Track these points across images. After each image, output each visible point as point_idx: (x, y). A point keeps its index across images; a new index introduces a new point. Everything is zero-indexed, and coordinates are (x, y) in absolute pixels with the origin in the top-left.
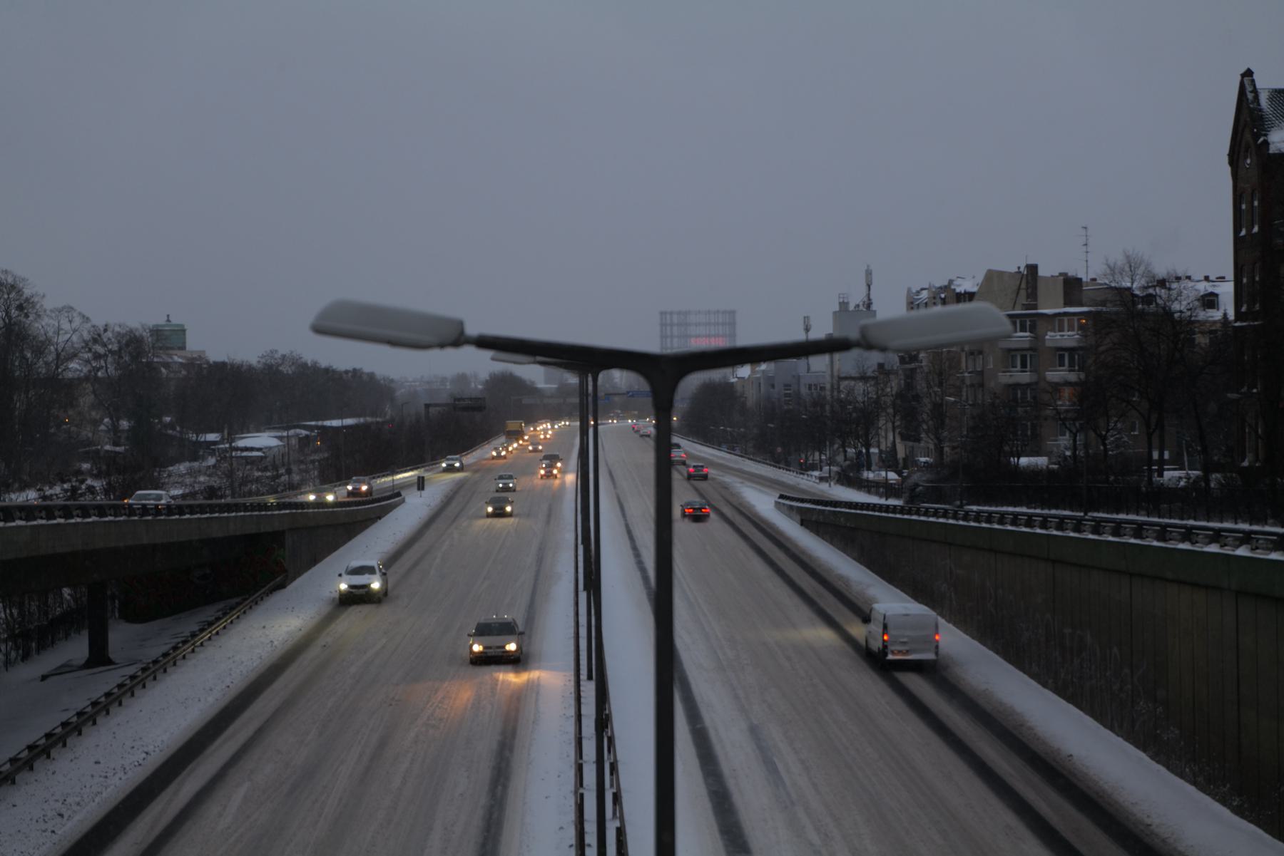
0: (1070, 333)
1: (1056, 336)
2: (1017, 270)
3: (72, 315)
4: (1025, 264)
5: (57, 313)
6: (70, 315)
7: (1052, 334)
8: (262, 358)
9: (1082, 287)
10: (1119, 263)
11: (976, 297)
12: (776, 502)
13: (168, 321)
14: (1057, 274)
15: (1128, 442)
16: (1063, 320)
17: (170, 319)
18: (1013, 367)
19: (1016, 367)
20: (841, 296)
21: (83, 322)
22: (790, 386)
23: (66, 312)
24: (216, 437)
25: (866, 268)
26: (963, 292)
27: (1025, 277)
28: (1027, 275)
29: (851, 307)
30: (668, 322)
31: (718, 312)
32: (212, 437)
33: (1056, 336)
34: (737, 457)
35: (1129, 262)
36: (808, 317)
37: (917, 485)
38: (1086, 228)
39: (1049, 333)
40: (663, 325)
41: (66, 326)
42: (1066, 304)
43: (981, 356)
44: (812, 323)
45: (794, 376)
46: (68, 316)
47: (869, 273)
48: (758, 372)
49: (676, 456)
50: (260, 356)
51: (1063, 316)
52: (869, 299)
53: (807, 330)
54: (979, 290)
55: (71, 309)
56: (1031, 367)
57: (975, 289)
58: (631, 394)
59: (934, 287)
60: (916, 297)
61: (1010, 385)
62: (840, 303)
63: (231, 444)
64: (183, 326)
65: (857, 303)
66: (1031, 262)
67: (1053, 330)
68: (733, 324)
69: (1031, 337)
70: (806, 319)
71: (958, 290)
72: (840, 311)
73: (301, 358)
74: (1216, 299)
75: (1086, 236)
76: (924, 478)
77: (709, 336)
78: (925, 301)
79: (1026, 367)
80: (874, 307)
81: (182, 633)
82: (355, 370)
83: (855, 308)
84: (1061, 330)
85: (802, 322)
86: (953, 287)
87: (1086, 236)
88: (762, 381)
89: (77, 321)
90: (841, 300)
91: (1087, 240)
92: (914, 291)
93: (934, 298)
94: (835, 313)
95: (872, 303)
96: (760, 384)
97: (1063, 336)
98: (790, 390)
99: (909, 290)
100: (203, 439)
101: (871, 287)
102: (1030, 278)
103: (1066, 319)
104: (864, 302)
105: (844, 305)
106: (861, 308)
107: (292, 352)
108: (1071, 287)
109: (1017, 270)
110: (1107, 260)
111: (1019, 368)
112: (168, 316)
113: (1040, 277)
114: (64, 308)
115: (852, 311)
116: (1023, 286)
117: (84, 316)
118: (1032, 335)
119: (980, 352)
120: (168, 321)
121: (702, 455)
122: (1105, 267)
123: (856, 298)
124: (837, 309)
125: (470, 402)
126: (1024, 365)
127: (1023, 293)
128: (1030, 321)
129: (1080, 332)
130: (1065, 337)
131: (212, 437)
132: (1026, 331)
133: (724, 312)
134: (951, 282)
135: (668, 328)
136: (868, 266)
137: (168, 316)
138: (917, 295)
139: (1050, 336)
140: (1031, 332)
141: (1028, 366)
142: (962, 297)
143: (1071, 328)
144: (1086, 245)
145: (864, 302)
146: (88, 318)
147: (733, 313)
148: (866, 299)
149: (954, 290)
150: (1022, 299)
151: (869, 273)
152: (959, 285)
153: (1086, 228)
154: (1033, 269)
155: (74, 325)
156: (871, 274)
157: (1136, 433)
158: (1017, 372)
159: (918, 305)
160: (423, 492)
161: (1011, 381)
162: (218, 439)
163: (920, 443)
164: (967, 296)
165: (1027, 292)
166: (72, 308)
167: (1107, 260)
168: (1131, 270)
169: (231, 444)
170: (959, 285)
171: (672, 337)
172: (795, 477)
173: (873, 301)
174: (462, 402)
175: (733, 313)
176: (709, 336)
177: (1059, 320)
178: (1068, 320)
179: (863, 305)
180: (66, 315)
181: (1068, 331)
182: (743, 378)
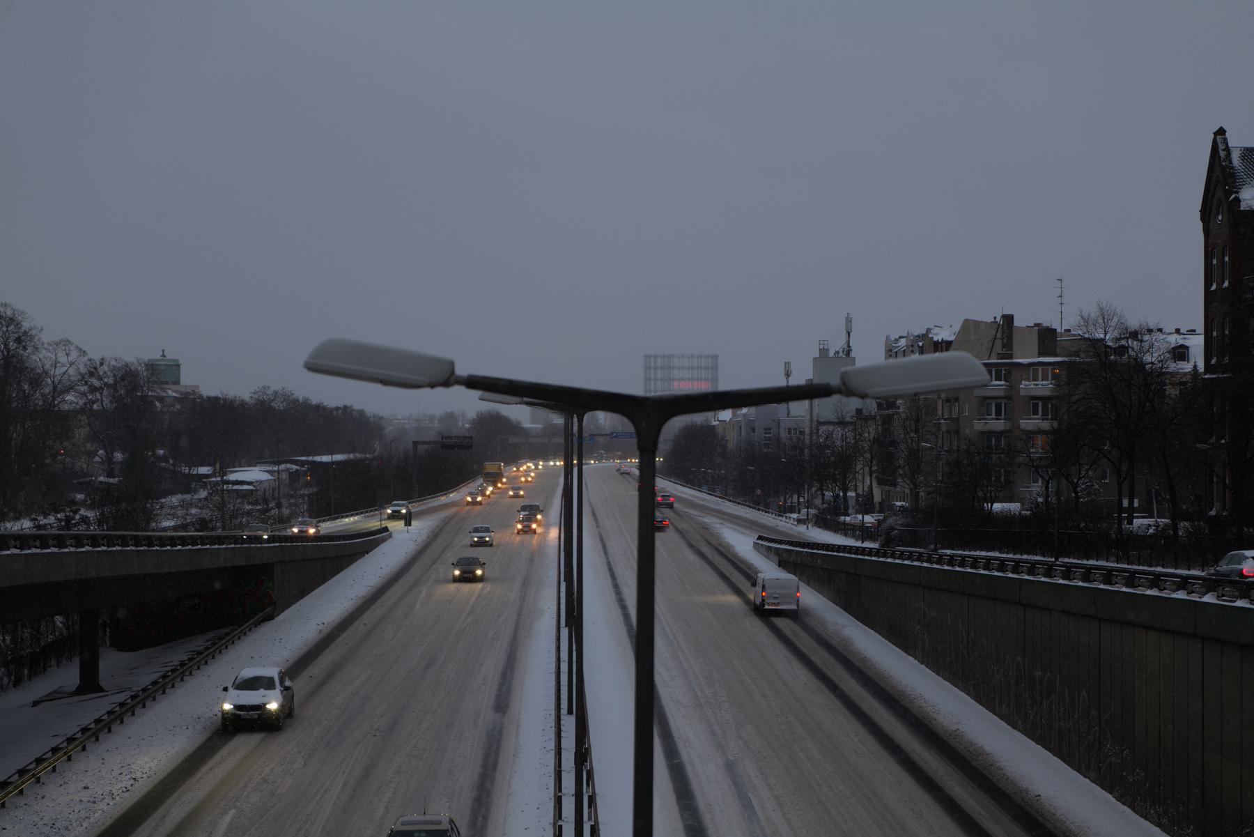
2: (993, 320)
5: (55, 346)
7: (1027, 383)
11: (953, 346)
13: (163, 355)
20: (822, 342)
23: (63, 345)
29: (831, 354)
32: (204, 470)
33: (1031, 385)
37: (892, 529)
40: (647, 368)
41: (63, 359)
42: (1040, 355)
44: (792, 367)
45: (774, 420)
47: (849, 321)
52: (849, 346)
53: (788, 375)
55: (67, 342)
56: (1005, 416)
57: (952, 338)
58: (615, 434)
62: (820, 349)
63: (222, 478)
67: (1028, 380)
68: (715, 368)
70: (787, 364)
73: (293, 394)
77: (692, 379)
78: (903, 349)
80: (853, 354)
81: (172, 662)
82: (345, 407)
83: (835, 354)
86: (930, 336)
89: (74, 355)
90: (822, 346)
92: (893, 339)
93: (912, 346)
95: (851, 350)
96: (741, 427)
97: (1038, 385)
98: (770, 433)
99: (888, 337)
100: (195, 472)
101: (851, 334)
103: (1040, 368)
105: (824, 351)
106: (841, 354)
107: (284, 389)
108: (1047, 337)
109: (993, 320)
111: (993, 416)
112: (163, 351)
114: (61, 341)
116: (999, 335)
117: (80, 350)
120: (163, 355)
123: (837, 344)
124: (818, 356)
126: (998, 412)
127: (999, 343)
130: (1040, 386)
131: (204, 470)
132: (1001, 380)
133: (708, 357)
134: (929, 330)
135: (652, 371)
137: (163, 351)
139: (1025, 385)
140: (1006, 380)
146: (84, 352)
147: (715, 357)
148: (845, 346)
149: (932, 338)
151: (849, 321)
152: (937, 334)
154: (1008, 319)
155: (71, 358)
156: (850, 321)
158: (992, 419)
159: (896, 352)
160: (409, 527)
161: (986, 428)
166: (69, 342)
170: (937, 334)
175: (715, 357)
176: (692, 379)
180: (63, 348)
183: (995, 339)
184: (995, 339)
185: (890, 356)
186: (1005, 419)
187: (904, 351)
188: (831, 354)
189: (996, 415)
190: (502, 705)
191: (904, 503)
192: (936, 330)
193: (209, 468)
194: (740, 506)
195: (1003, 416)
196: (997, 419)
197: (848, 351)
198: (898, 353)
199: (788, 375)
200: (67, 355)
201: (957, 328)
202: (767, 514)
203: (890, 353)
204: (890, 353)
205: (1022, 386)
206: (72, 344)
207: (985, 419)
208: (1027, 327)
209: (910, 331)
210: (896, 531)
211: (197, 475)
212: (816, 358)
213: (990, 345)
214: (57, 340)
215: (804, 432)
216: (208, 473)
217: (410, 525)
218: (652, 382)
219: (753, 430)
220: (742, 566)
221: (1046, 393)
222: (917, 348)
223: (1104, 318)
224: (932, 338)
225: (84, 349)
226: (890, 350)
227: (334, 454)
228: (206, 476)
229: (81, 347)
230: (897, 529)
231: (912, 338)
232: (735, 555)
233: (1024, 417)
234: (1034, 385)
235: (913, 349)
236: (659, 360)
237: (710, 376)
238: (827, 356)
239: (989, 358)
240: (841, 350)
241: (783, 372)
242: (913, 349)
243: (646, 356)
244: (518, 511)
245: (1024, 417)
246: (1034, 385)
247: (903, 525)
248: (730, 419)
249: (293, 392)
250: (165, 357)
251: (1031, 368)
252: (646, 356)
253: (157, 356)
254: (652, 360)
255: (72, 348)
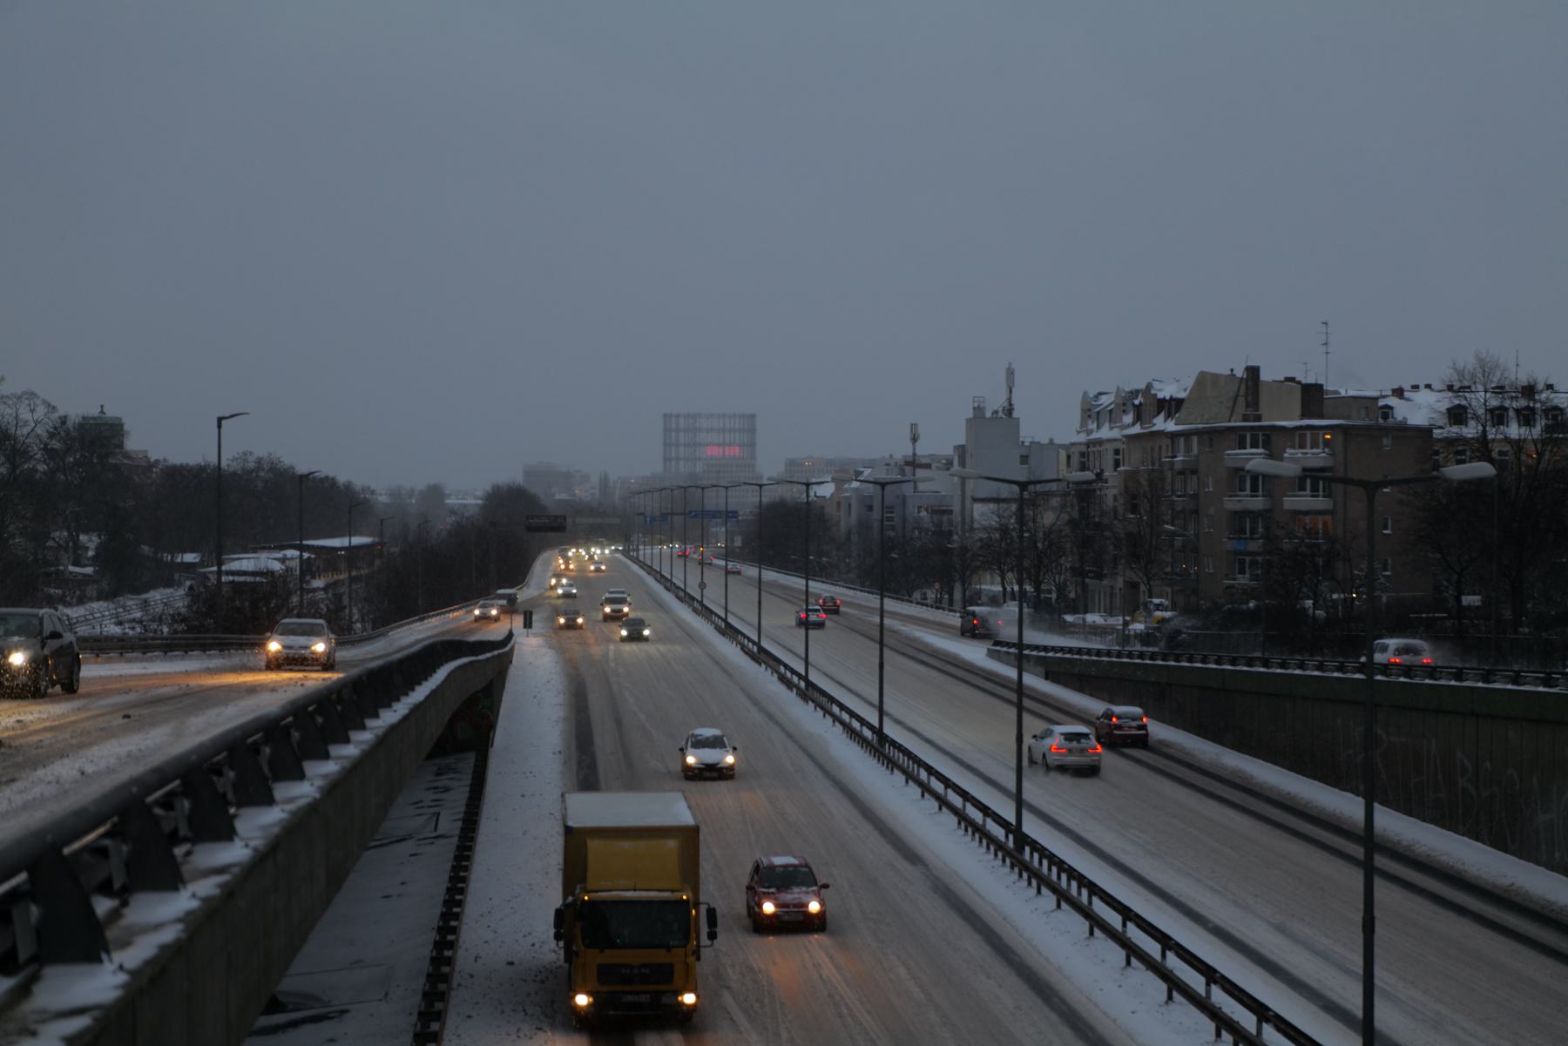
0: (1314, 451)
1: (1297, 454)
2: (1229, 373)
3: (34, 403)
4: (1244, 366)
5: (15, 400)
6: (32, 403)
7: (1293, 451)
8: (232, 460)
9: (1323, 395)
10: (1470, 367)
11: (1185, 406)
12: (989, 650)
13: (102, 412)
14: (1282, 379)
15: (1384, 584)
16: (1305, 434)
17: (105, 410)
18: (1241, 490)
19: (1245, 490)
20: (976, 399)
21: (48, 412)
22: (892, 507)
23: (26, 399)
24: (195, 558)
25: (1007, 366)
26: (1168, 398)
27: (1244, 381)
28: (1247, 379)
29: (988, 415)
30: (674, 426)
31: (734, 415)
32: (190, 558)
33: (1297, 454)
34: (866, 594)
35: (1483, 368)
36: (916, 425)
37: (1179, 632)
38: (1326, 323)
39: (1288, 450)
40: (667, 430)
41: (25, 415)
42: (1304, 416)
43: (1195, 477)
44: (921, 430)
45: (898, 497)
46: (30, 405)
47: (1010, 373)
48: (846, 490)
49: (812, 588)
50: (231, 458)
51: (1306, 430)
52: (1011, 405)
53: (914, 439)
54: (1188, 396)
55: (33, 395)
56: (1263, 491)
57: (1182, 395)
58: (693, 513)
59: (1124, 391)
60: (1094, 403)
61: (1236, 512)
62: (974, 408)
63: (219, 567)
64: (120, 419)
65: (996, 408)
66: (1251, 363)
67: (1293, 447)
68: (753, 431)
69: (1266, 455)
70: (914, 426)
71: (1160, 396)
72: (975, 417)
73: (280, 462)
74: (1390, 411)
75: (1327, 333)
76: (1188, 624)
77: (723, 445)
78: (1109, 408)
79: (1318, 491)
80: (1015, 414)
81: (421, 801)
82: (333, 479)
83: (993, 414)
84: (1302, 446)
85: (909, 430)
86: (1153, 392)
87: (1327, 333)
88: (854, 503)
89: (41, 411)
90: (976, 405)
91: (1327, 338)
92: (1092, 396)
93: (1124, 404)
94: (968, 421)
95: (1013, 409)
96: (850, 505)
97: (1307, 453)
98: (892, 512)
99: (1085, 394)
100: (179, 560)
101: (1013, 389)
102: (1250, 383)
103: (1308, 433)
104: (1004, 407)
105: (979, 410)
106: (1000, 414)
107: (270, 454)
108: (1312, 397)
109: (1229, 373)
110: (1454, 364)
111: (1248, 492)
112: (102, 407)
113: (1263, 381)
114: (25, 393)
115: (990, 418)
116: (1242, 391)
117: (49, 405)
118: (1267, 452)
119: (1194, 472)
120: (102, 412)
121: (796, 586)
122: (1452, 371)
123: (996, 401)
124: (971, 415)
125: (546, 521)
126: (1254, 489)
127: (1241, 400)
128: (1264, 435)
129: (1326, 450)
130: (1308, 455)
131: (190, 558)
132: (1258, 448)
133: (743, 416)
134: (1149, 386)
135: (673, 434)
136: (1010, 364)
137: (102, 407)
138: (1096, 401)
139: (1290, 454)
140: (1264, 447)
141: (1260, 489)
142: (1167, 404)
143: (1314, 445)
144: (1326, 344)
145: (1004, 407)
146: (54, 408)
147: (752, 417)
148: (1006, 404)
149: (1156, 395)
150: (1241, 408)
151: (1010, 373)
152: (1160, 390)
153: (1326, 323)
154: (1253, 372)
155: (36, 416)
156: (1013, 373)
157: (1388, 573)
158: (1247, 496)
159: (1098, 413)
160: (530, 630)
161: (1239, 507)
162: (197, 560)
163: (1101, 580)
164: (1173, 403)
165: (1246, 399)
166: (33, 394)
167: (1454, 364)
168: (1484, 376)
169: (219, 567)
170: (1160, 390)
171: (678, 445)
172: (947, 615)
173: (1015, 407)
174: (536, 520)
175: (752, 417)
176: (723, 445)
177: (1300, 435)
178: (1312, 434)
179: (1003, 411)
180: (27, 402)
181: (1312, 448)
182: (824, 497)
183: (1237, 396)
184: (1237, 396)
185: (1089, 416)
186: (1263, 496)
187: (1111, 411)
188: (988, 415)
189: (1312, 491)
190: (912, 857)
191: (1163, 600)
192: (1156, 385)
193: (194, 555)
194: (904, 603)
195: (1260, 493)
196: (1251, 496)
197: (1009, 411)
198: (1101, 416)
199: (914, 439)
200: (32, 411)
201: (1190, 382)
202: (952, 613)
203: (1089, 413)
204: (1089, 413)
205: (1286, 455)
206: (39, 397)
207: (1236, 496)
208: (1274, 381)
209: (1121, 386)
210: (1184, 636)
211: (182, 563)
212: (970, 419)
213: (1231, 404)
214: (19, 392)
215: (952, 511)
216: (195, 561)
217: (530, 627)
218: (673, 448)
219: (870, 508)
220: (990, 677)
221: (1320, 464)
222: (1132, 407)
223: (1484, 371)
224: (1156, 395)
225: (53, 404)
226: (1089, 410)
227: (354, 535)
228: (192, 566)
229: (50, 400)
230: (1185, 633)
231: (1123, 395)
232: (963, 661)
233: (1289, 493)
234: (1303, 453)
235: (1124, 408)
236: (682, 421)
237: (746, 441)
238: (983, 417)
239: (1229, 421)
240: (1000, 409)
241: (908, 436)
242: (1124, 408)
243: (665, 415)
244: (602, 604)
245: (1289, 493)
246: (1303, 453)
247: (1193, 628)
248: (832, 495)
249: (281, 459)
250: (104, 413)
251: (1298, 433)
252: (665, 415)
253: (95, 412)
254: (673, 419)
255: (37, 402)
